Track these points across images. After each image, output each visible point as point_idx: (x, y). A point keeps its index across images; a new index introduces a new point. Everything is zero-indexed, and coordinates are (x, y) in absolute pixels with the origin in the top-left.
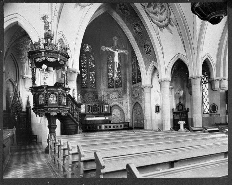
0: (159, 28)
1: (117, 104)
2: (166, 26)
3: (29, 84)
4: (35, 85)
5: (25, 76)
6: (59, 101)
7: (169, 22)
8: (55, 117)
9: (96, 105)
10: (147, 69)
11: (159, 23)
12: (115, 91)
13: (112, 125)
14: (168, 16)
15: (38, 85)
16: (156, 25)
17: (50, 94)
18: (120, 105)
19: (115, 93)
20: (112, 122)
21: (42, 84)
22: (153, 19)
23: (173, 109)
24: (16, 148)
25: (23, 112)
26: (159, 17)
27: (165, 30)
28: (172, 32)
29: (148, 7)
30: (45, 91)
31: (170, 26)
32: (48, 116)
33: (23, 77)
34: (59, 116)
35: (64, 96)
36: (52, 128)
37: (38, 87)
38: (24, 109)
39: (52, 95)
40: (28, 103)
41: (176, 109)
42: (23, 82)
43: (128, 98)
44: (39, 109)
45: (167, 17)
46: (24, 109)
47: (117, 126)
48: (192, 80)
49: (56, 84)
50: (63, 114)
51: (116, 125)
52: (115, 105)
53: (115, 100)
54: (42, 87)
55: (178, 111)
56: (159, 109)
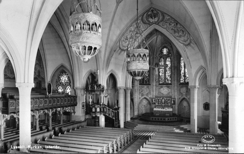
0: (185, 47)
2: (189, 44)
7: (191, 42)
9: (164, 99)
10: (3, 119)
11: (184, 43)
13: (154, 118)
14: (189, 37)
16: (182, 45)
22: (180, 40)
23: (222, 108)
26: (182, 39)
27: (189, 47)
28: (195, 49)
29: (174, 34)
31: (192, 44)
37: (180, 59)
41: (225, 108)
45: (188, 39)
47: (161, 119)
48: (191, 89)
51: (157, 118)
55: (226, 111)
56: (179, 107)
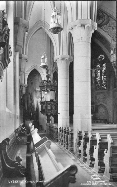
1: (103, 103)
3: (39, 100)
4: (41, 134)
5: (37, 90)
6: (52, 108)
8: (50, 116)
12: (102, 93)
15: (43, 101)
17: (48, 105)
18: (104, 104)
19: (101, 95)
20: (98, 118)
21: (45, 101)
24: (64, 130)
25: (35, 111)
30: (46, 104)
32: (47, 115)
33: (35, 91)
34: (52, 115)
35: (54, 105)
36: (49, 120)
38: (35, 110)
39: (49, 105)
40: (37, 106)
42: (35, 94)
43: (111, 98)
44: (43, 111)
46: (35, 110)
49: (51, 100)
50: (54, 114)
52: (101, 104)
53: (101, 100)
54: (44, 102)
